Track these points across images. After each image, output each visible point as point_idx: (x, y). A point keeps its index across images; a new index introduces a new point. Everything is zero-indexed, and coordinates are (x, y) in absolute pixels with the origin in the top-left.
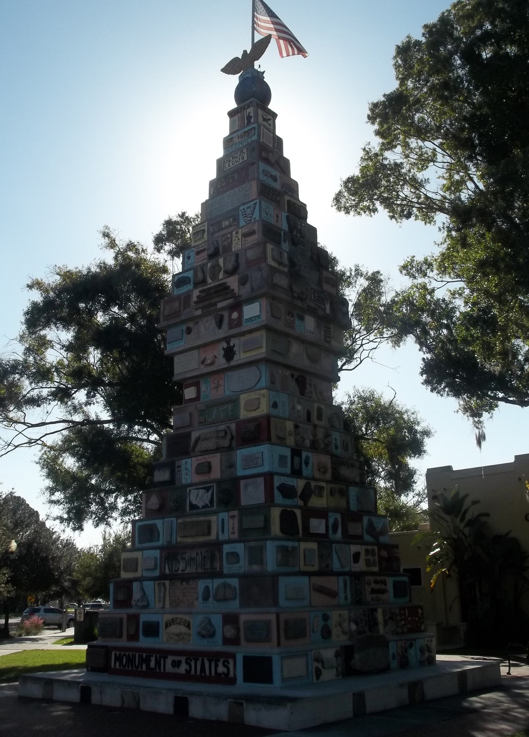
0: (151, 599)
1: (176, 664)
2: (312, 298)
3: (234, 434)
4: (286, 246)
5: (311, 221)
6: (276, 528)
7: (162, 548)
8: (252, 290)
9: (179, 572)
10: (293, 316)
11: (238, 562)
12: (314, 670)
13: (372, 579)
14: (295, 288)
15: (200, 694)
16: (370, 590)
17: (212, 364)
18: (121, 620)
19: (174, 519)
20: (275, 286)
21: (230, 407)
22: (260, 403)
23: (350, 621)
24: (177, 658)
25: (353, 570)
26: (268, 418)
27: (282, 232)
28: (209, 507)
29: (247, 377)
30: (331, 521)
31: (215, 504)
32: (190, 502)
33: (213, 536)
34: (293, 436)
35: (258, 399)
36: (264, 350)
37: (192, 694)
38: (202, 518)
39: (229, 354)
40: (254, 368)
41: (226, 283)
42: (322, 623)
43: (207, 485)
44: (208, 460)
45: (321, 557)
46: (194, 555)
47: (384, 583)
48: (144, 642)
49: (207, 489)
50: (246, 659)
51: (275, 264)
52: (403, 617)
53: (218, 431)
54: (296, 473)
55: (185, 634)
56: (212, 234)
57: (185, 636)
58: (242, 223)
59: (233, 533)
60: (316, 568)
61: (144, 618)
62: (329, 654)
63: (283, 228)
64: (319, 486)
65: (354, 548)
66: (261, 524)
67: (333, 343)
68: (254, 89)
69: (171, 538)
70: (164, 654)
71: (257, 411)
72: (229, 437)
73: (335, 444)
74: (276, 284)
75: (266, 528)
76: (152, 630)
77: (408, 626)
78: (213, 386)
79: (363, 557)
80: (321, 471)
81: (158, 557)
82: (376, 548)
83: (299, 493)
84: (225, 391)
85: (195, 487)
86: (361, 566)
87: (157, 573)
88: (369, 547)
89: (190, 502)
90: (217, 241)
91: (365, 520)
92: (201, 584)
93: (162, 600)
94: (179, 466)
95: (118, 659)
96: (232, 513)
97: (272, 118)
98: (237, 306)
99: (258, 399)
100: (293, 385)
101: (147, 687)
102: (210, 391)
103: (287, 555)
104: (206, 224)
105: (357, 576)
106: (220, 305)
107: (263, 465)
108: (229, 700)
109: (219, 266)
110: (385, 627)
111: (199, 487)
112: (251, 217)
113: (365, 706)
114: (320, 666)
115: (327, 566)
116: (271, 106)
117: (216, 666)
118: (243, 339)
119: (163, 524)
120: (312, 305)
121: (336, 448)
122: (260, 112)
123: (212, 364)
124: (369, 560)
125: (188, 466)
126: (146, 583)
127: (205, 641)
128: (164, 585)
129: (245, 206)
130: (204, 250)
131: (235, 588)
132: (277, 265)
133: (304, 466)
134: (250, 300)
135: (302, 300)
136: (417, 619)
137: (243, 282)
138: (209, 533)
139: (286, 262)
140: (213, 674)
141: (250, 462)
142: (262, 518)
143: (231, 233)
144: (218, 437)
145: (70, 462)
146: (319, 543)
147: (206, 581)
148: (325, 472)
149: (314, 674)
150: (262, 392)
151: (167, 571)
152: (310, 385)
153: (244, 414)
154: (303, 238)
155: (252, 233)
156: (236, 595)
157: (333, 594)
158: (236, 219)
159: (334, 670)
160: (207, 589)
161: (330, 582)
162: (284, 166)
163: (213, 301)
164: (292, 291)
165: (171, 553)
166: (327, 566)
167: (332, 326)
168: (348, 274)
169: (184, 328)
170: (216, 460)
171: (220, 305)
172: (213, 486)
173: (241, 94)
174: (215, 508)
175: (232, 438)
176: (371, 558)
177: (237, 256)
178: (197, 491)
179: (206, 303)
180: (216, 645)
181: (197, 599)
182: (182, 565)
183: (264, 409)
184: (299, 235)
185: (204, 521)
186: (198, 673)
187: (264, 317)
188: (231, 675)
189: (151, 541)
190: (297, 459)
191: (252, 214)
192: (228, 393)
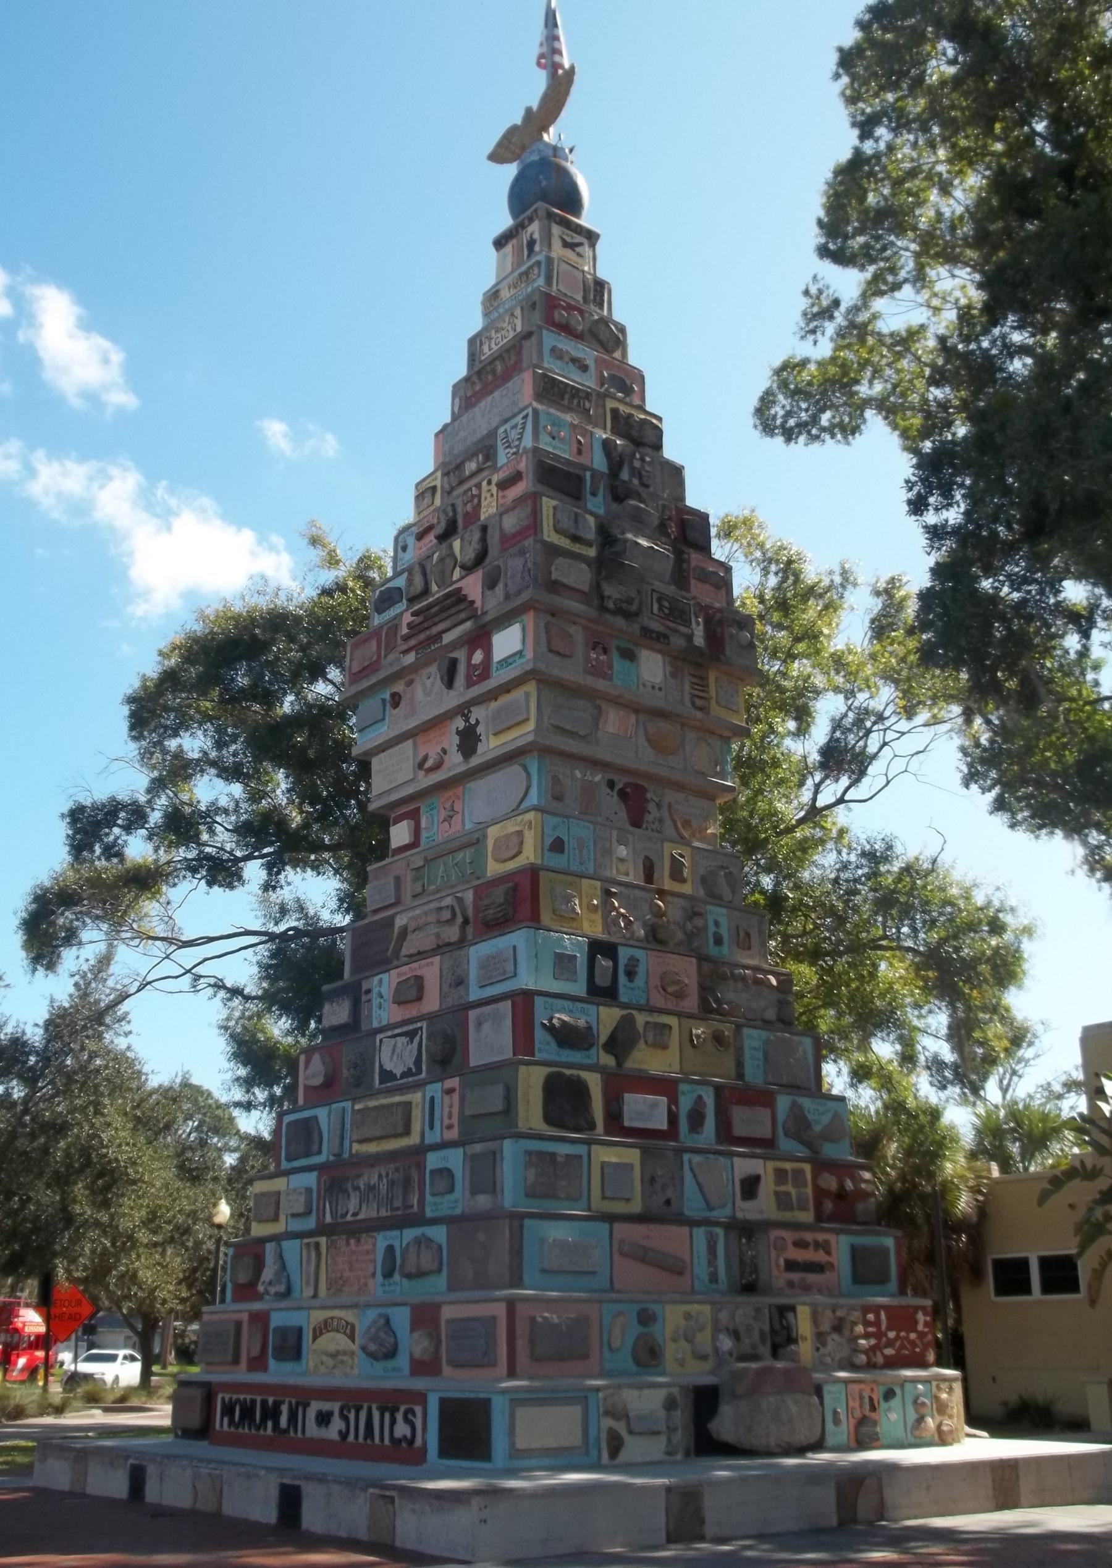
0: (295, 1278)
1: (324, 1419)
2: (655, 610)
3: (470, 912)
4: (597, 504)
5: (671, 451)
6: (531, 1111)
7: (320, 1168)
8: (507, 597)
9: (349, 1218)
10: (605, 651)
11: (451, 1190)
12: (604, 1436)
13: (788, 1236)
14: (608, 590)
15: (322, 1479)
16: (782, 1262)
17: (438, 766)
18: (238, 1325)
19: (348, 1105)
20: (554, 587)
21: (467, 855)
22: (522, 843)
23: (717, 1329)
24: (326, 1406)
25: (740, 1215)
26: (533, 873)
27: (588, 474)
28: (413, 1075)
29: (503, 786)
30: (685, 1104)
31: (424, 1068)
32: (381, 1066)
33: (414, 1139)
34: (600, 912)
35: (520, 833)
36: (531, 726)
37: (309, 1477)
38: (397, 1099)
39: (469, 740)
40: (514, 771)
41: (460, 589)
42: (635, 1329)
43: (411, 1027)
44: (419, 973)
45: (650, 1181)
46: (374, 1180)
47: (826, 1247)
48: (278, 1373)
49: (411, 1035)
50: (445, 1404)
51: (564, 542)
52: (871, 1329)
53: (440, 909)
54: (602, 993)
55: (345, 1353)
56: (449, 493)
57: (345, 1358)
58: (502, 459)
59: (450, 1127)
60: (636, 1207)
61: (277, 1320)
62: (646, 1400)
63: (596, 466)
64: (656, 1024)
65: (744, 1167)
66: (498, 1105)
67: (716, 710)
68: (544, 183)
69: (342, 1144)
70: (303, 1396)
71: (517, 860)
72: (460, 920)
73: (715, 933)
74: (556, 582)
75: (509, 1110)
76: (291, 1346)
77: (889, 1351)
78: (443, 814)
79: (767, 1186)
80: (670, 989)
81: (315, 1188)
82: (807, 1168)
83: (603, 1038)
84: (464, 824)
85: (390, 1033)
86: (763, 1206)
87: (310, 1223)
88: (788, 1166)
89: (381, 1066)
90: (453, 505)
91: (783, 1102)
92: (382, 1241)
93: (312, 1279)
94: (369, 991)
95: (228, 1410)
96: (450, 1083)
97: (585, 241)
98: (481, 638)
99: (520, 833)
100: (611, 802)
101: (235, 1464)
102: (436, 828)
103: (551, 1177)
104: (439, 474)
105: (747, 1230)
106: (447, 638)
107: (515, 975)
108: (371, 1490)
109: (452, 555)
110: (818, 1349)
111: (397, 1031)
112: (517, 447)
113: (702, 1521)
114: (621, 1427)
115: (668, 1202)
116: (585, 220)
117: (393, 1422)
118: (494, 705)
119: (329, 1116)
120: (655, 626)
121: (719, 941)
122: (556, 230)
123: (438, 766)
124: (788, 1194)
125: (384, 990)
126: (286, 1244)
127: (380, 1367)
128: (317, 1245)
129: (507, 426)
130: (430, 528)
131: (440, 1247)
132: (568, 541)
133: (622, 978)
134: (504, 620)
135: (628, 615)
136: (913, 1336)
137: (490, 583)
138: (407, 1132)
139: (591, 534)
140: (387, 1441)
141: (494, 969)
142: (500, 1090)
143: (478, 486)
144: (439, 922)
145: (278, 1028)
146: (645, 1151)
147: (389, 1234)
148: (680, 995)
149: (604, 1445)
150: (530, 816)
151: (328, 1219)
152: (659, 806)
153: (493, 868)
154: (647, 486)
155: (516, 478)
156: (441, 1263)
157: (675, 1268)
158: (489, 453)
159: (662, 1441)
160: (390, 1249)
161: (669, 1239)
162: (610, 339)
163: (435, 630)
164: (602, 598)
165: (337, 1178)
166: (668, 1202)
167: (712, 676)
168: (826, 582)
169: (387, 696)
170: (431, 971)
171: (447, 638)
172: (421, 1028)
173: (521, 198)
174: (423, 1075)
175: (466, 922)
176: (793, 1191)
177: (484, 529)
178: (393, 1041)
179: (422, 636)
180: (396, 1376)
181: (374, 1275)
182: (353, 1204)
183: (529, 855)
184: (636, 481)
185: (398, 1104)
186: (361, 1439)
187: (529, 654)
188: (418, 1442)
189: (308, 1154)
190: (604, 963)
191: (520, 439)
192: (468, 826)
